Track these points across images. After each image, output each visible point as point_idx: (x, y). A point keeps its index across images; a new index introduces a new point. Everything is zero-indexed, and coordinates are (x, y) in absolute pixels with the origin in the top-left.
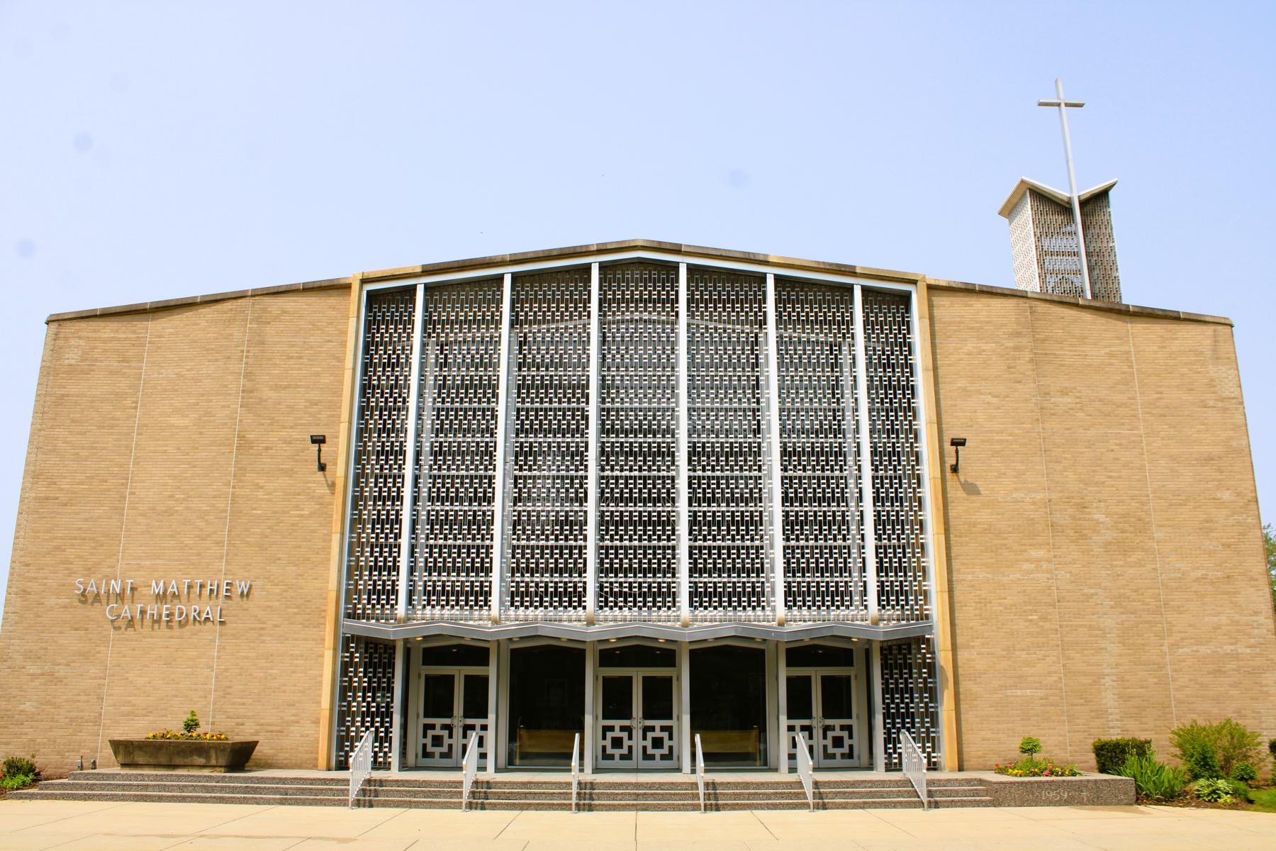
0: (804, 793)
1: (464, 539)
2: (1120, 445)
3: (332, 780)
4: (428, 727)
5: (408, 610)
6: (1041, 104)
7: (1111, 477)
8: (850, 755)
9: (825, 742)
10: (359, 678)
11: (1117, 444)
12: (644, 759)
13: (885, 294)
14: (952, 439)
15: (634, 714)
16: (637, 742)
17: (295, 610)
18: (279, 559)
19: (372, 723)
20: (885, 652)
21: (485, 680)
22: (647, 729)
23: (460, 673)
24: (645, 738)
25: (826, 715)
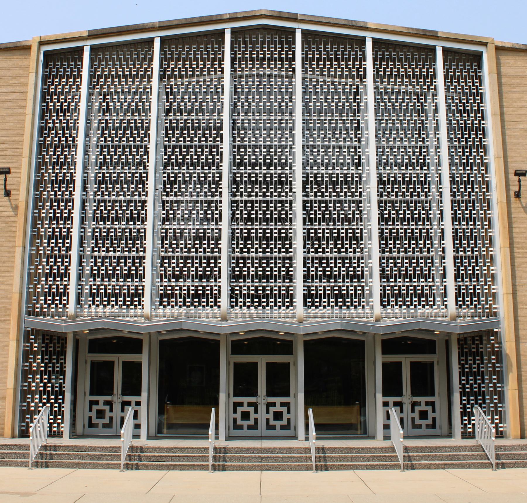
0: (396, 456)
4: (93, 403)
5: (77, 308)
8: (433, 426)
16: (262, 415)
20: (461, 342)
22: (269, 405)
24: (268, 412)
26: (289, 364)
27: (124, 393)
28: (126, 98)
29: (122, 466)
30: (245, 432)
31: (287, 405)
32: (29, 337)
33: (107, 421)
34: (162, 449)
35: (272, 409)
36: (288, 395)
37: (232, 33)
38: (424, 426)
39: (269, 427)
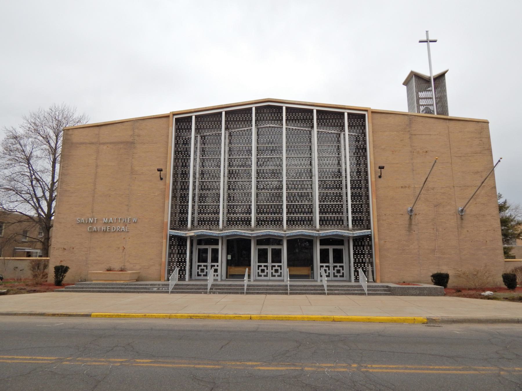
0: (324, 289)
1: (337, 202)
2: (443, 167)
3: (165, 284)
4: (199, 266)
5: (191, 227)
6: (420, 42)
7: (439, 179)
8: (343, 276)
9: (334, 271)
10: (176, 250)
11: (441, 168)
12: (272, 276)
13: (356, 115)
14: (379, 167)
15: (269, 261)
16: (270, 271)
17: (153, 227)
18: (147, 210)
19: (180, 265)
20: (354, 241)
21: (217, 250)
22: (273, 266)
23: (210, 248)
24: (272, 269)
25: (334, 262)
26: (342, 249)
27: (212, 262)
28: (244, 137)
29: (170, 292)
30: (263, 278)
31: (280, 266)
32: (171, 239)
33: (265, 274)
34: (236, 285)
35: (336, 269)
36: (281, 262)
37: (256, 109)
38: (339, 276)
39: (335, 276)
